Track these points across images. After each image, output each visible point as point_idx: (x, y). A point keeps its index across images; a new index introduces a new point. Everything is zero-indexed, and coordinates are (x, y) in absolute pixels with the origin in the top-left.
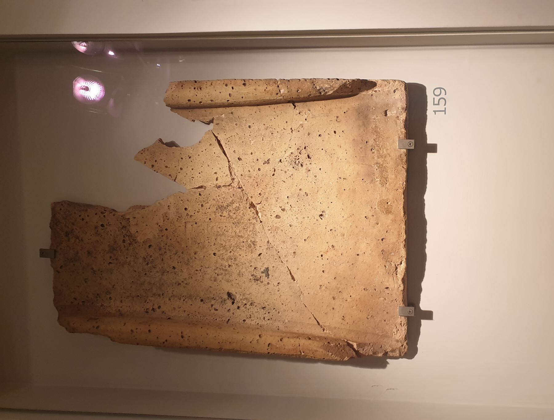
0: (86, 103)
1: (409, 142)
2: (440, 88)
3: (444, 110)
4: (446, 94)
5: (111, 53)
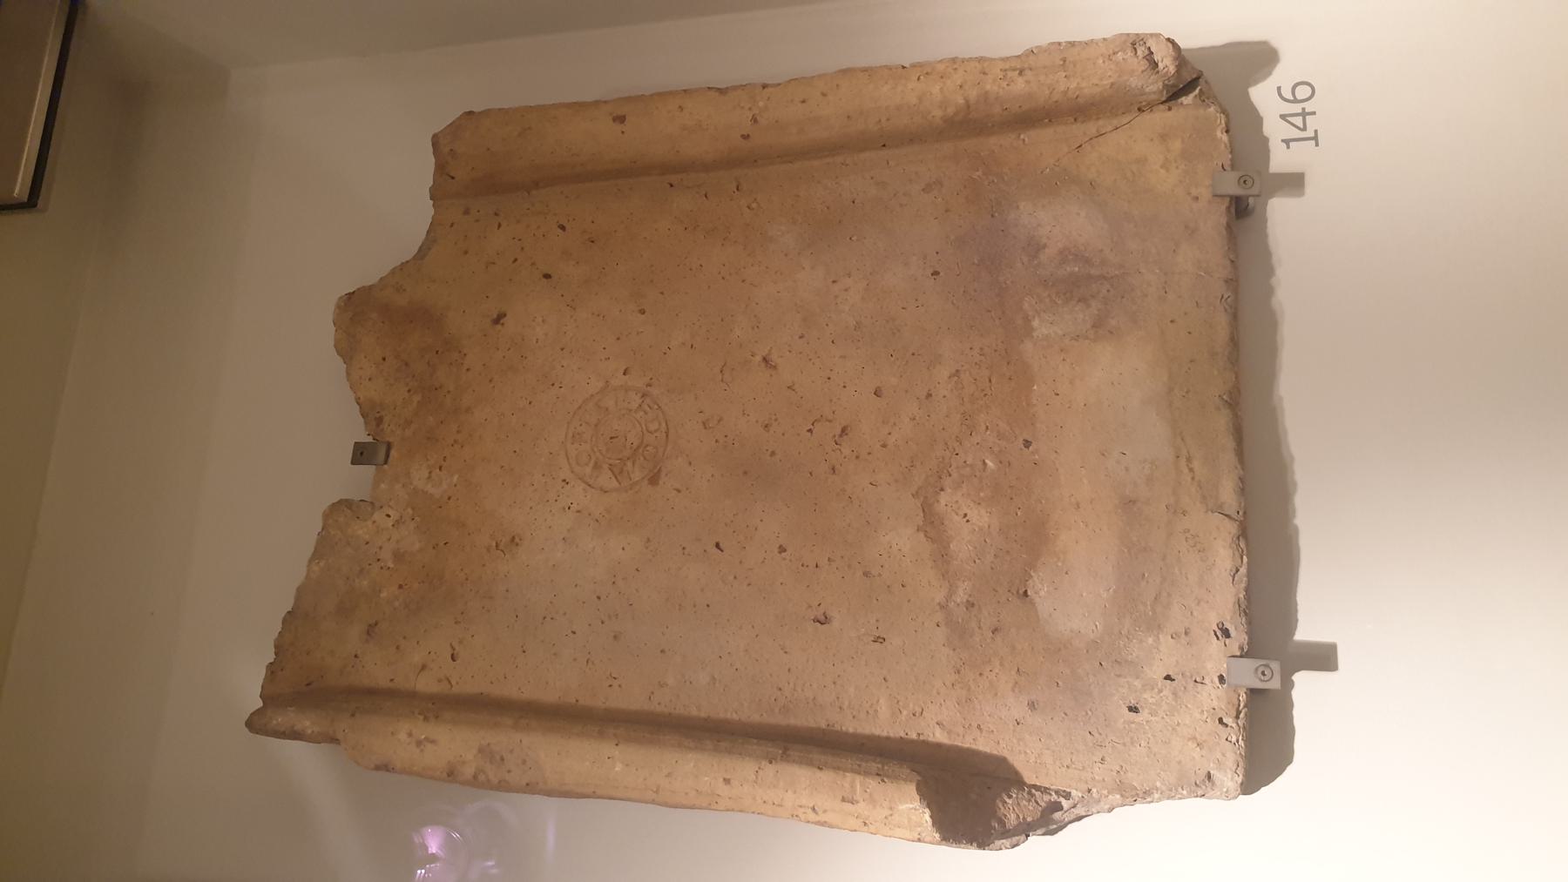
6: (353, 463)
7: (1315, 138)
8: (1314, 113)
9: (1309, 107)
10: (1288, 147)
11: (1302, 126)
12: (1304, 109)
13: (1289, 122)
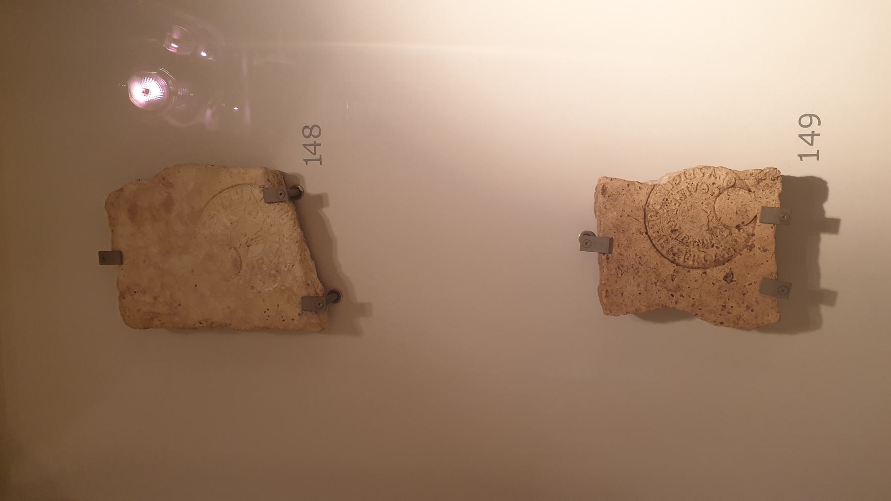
0: (152, 106)
1: (589, 240)
2: (811, 116)
3: (816, 153)
4: (819, 124)
5: (204, 54)
6: (581, 250)
7: (320, 160)
8: (818, 135)
9: (318, 141)
10: (801, 160)
11: (810, 143)
12: (315, 142)
13: (307, 149)
